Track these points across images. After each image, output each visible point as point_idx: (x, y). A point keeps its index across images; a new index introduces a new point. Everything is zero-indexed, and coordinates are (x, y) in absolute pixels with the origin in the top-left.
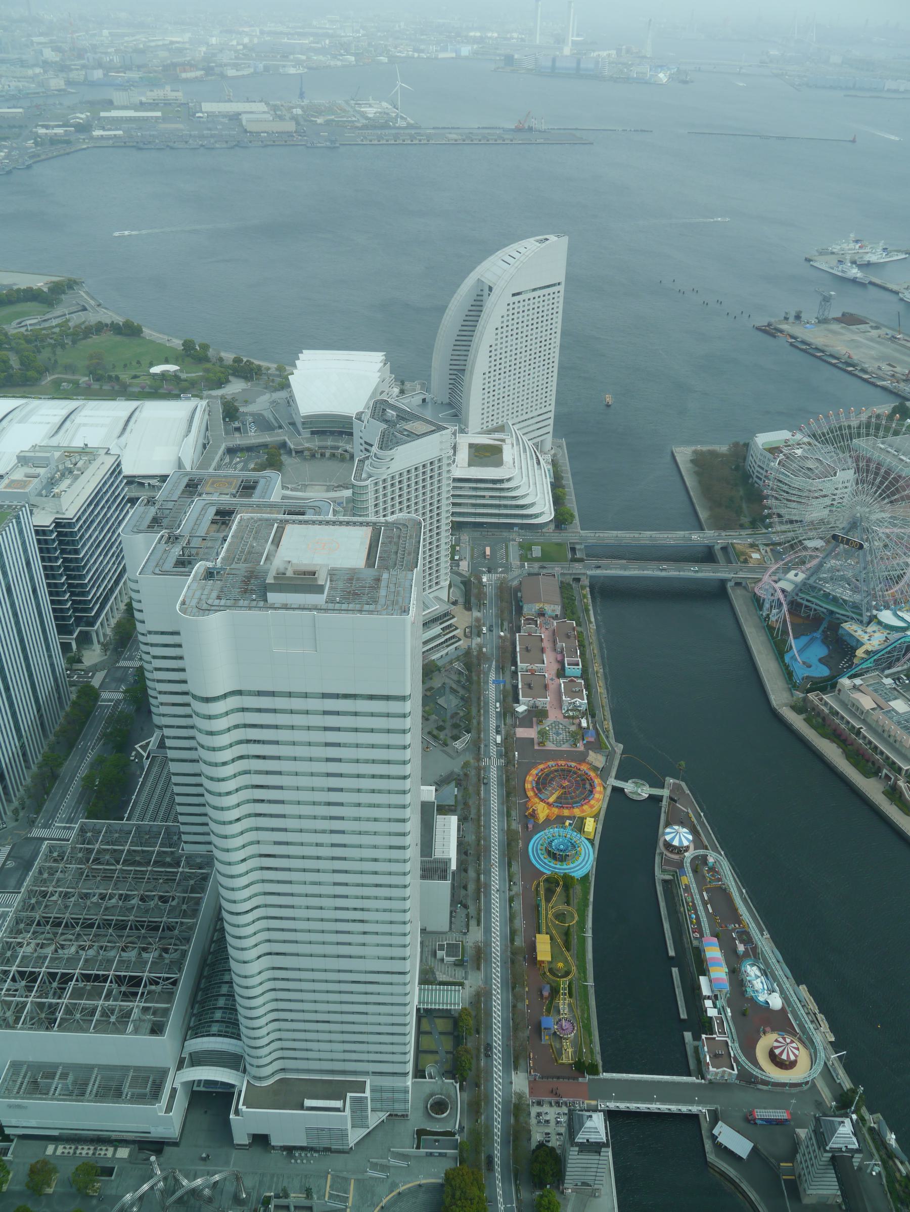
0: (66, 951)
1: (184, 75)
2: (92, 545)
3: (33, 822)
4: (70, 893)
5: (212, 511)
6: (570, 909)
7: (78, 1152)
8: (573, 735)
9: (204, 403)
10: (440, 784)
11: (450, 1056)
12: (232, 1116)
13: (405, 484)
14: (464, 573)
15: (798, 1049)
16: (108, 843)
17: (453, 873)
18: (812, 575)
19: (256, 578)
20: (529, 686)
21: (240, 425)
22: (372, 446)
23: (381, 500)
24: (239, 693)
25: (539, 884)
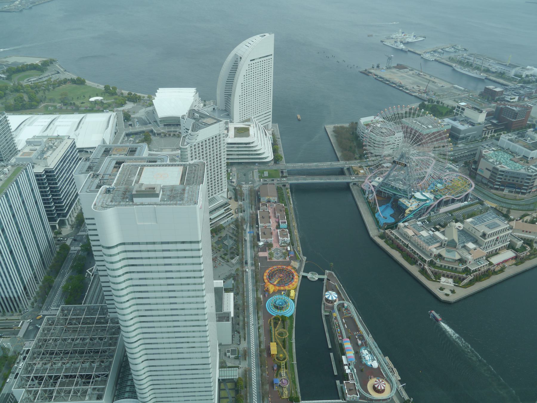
0: (56, 365)
2: (63, 180)
3: (41, 308)
6: (285, 330)
8: (284, 254)
9: (115, 114)
10: (225, 280)
13: (204, 146)
16: (75, 315)
17: (232, 318)
18: (386, 178)
19: (129, 192)
20: (264, 234)
21: (132, 123)
23: (194, 154)
24: (124, 244)
25: (271, 321)
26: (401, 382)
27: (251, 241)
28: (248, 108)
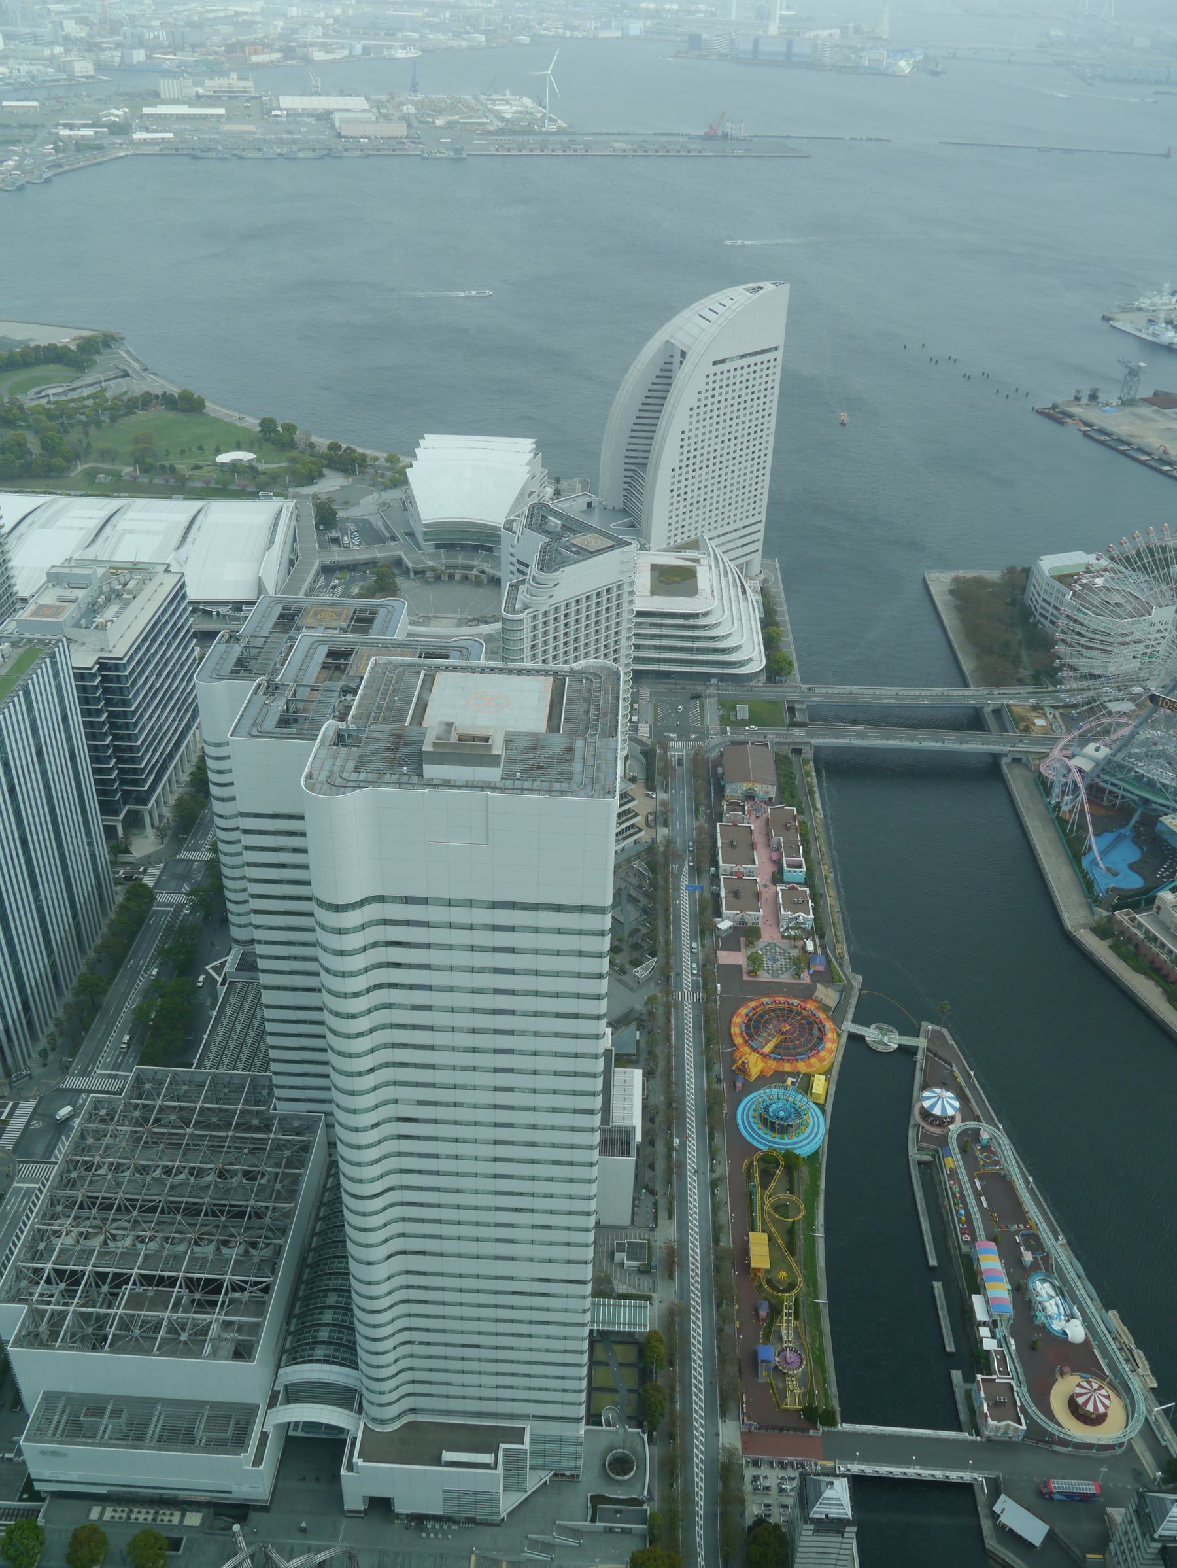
0: (119, 1244)
1: (254, 59)
3: (67, 1068)
4: (123, 1165)
5: (323, 651)
6: (794, 1198)
7: (133, 1516)
8: (796, 962)
9: (290, 504)
11: (633, 1396)
12: (343, 1472)
13: (572, 619)
14: (644, 739)
15: (1108, 1398)
19: (406, 743)
20: (735, 894)
22: (527, 566)
23: (540, 641)
24: (381, 899)
25: (751, 1165)
26: (1160, 1395)
27: (692, 916)
28: (694, 507)
